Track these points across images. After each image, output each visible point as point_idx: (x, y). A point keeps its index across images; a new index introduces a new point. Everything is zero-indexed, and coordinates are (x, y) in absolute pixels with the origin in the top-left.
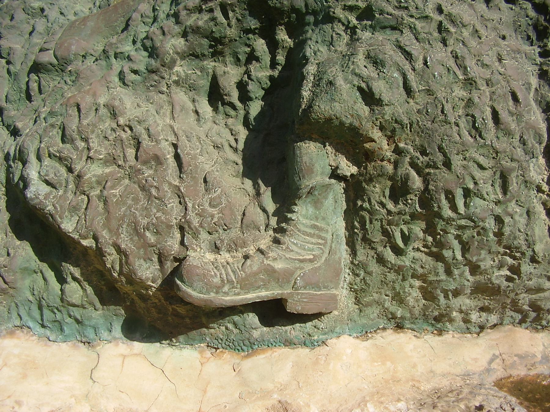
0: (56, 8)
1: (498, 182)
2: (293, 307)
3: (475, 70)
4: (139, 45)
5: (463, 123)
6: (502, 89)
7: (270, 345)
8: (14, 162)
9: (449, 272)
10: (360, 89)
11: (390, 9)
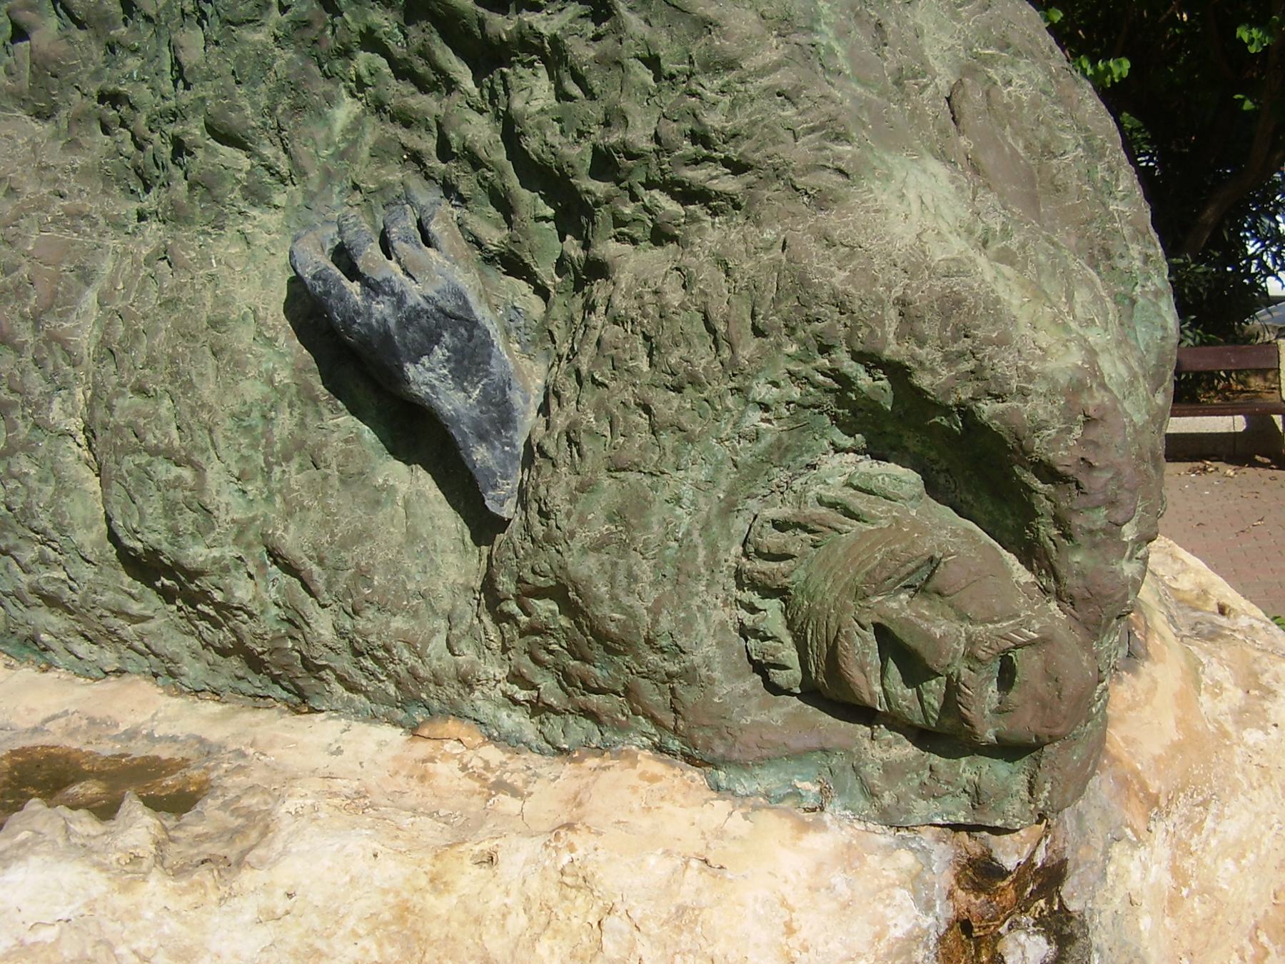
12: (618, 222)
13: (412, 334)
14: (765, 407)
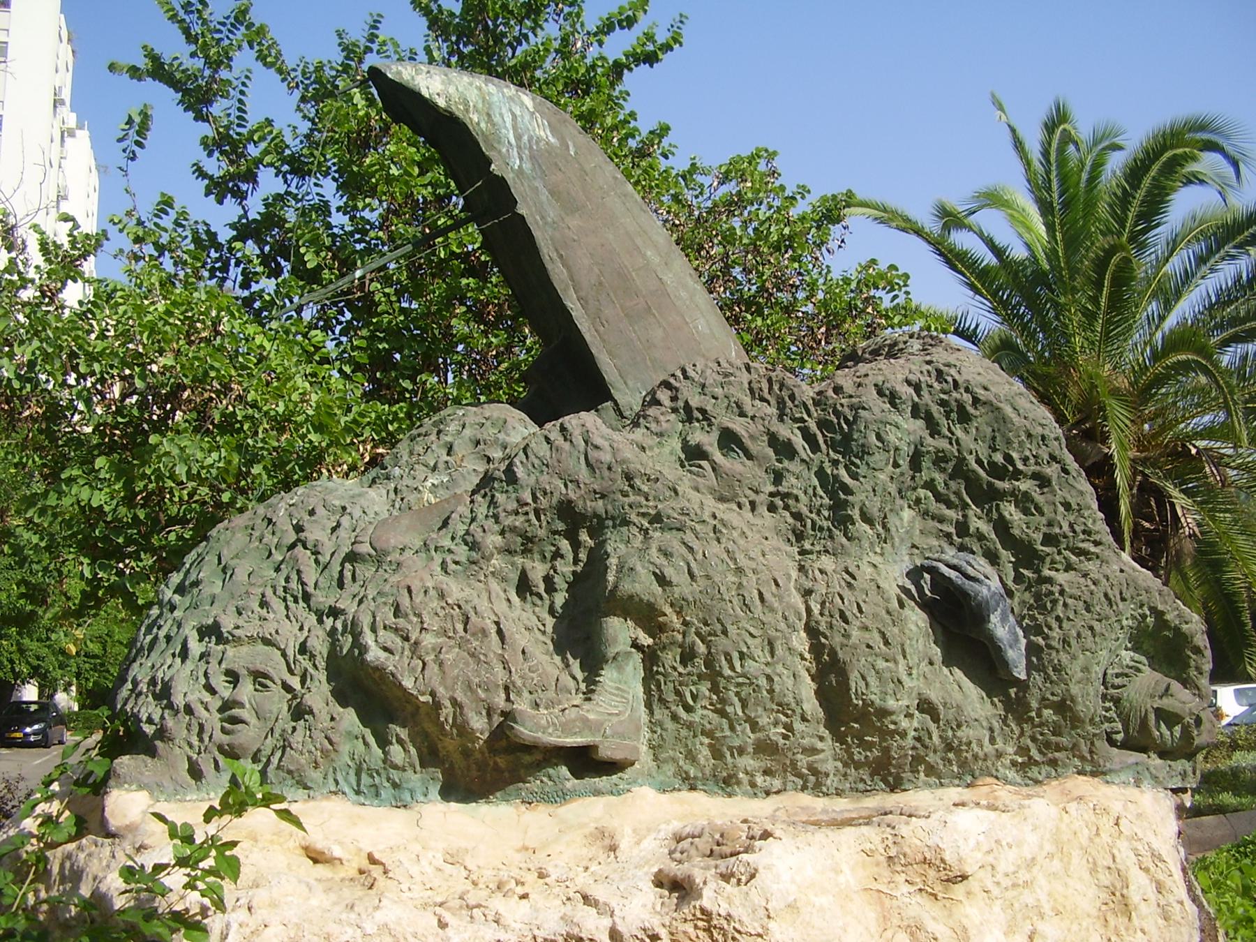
0: (358, 507)
1: (767, 648)
3: (743, 561)
4: (458, 540)
5: (735, 600)
6: (766, 576)
8: (342, 635)
9: (732, 728)
10: (654, 574)
11: (676, 515)
12: (1053, 562)
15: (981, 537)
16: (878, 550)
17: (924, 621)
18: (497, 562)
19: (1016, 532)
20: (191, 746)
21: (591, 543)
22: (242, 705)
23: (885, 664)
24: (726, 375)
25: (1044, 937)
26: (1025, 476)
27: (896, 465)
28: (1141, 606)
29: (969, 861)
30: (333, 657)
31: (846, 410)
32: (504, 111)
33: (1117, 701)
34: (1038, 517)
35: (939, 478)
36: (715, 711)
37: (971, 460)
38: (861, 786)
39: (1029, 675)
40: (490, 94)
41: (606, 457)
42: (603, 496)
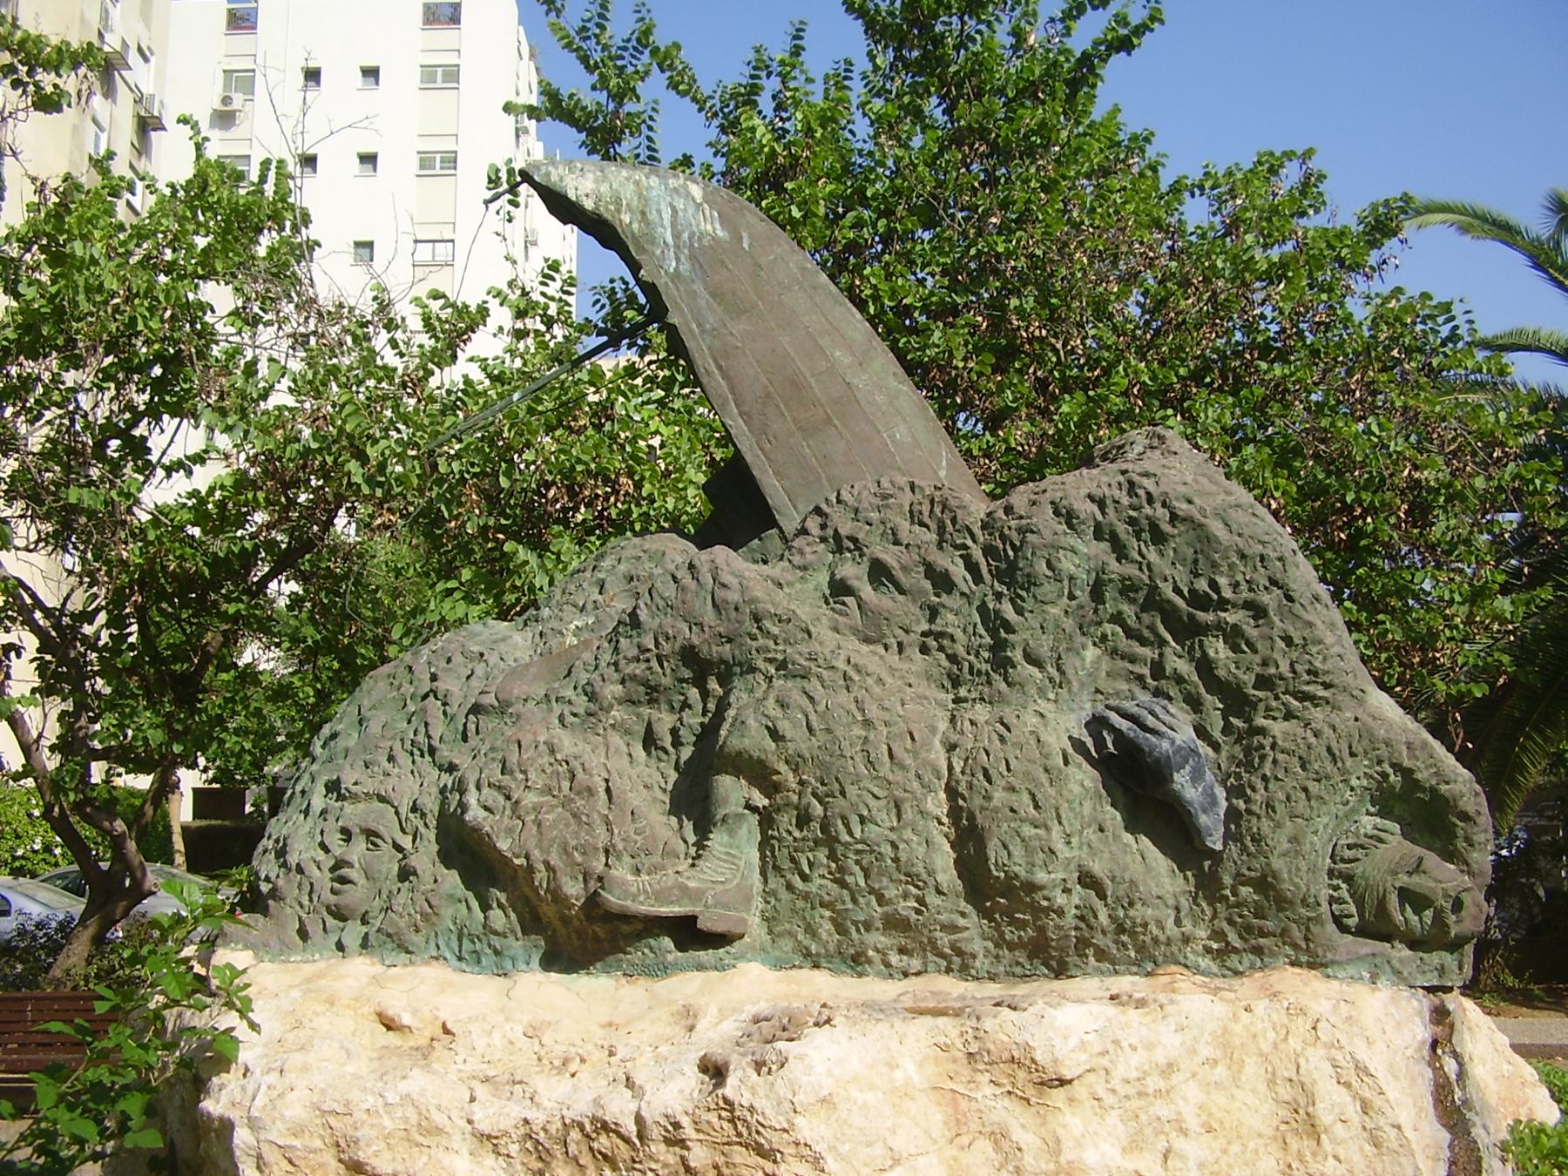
2: (704, 924)
3: (873, 711)
4: (580, 690)
5: (860, 755)
7: (679, 968)
9: (854, 901)
10: (767, 727)
12: (1268, 709)
13: (1178, 759)
14: (1352, 789)
15: (1179, 679)
16: (1052, 696)
17: (1093, 780)
18: (617, 713)
19: (1221, 673)
20: (302, 906)
21: (720, 691)
22: (351, 865)
23: (1034, 831)
24: (885, 497)
25: (1183, 1158)
26: (1234, 606)
27: (1072, 597)
28: (1380, 762)
29: (1067, 1062)
30: (443, 816)
31: (1014, 535)
32: (663, 206)
33: (1349, 879)
34: (1250, 656)
35: (1128, 610)
36: (834, 881)
37: (1167, 590)
38: (1018, 970)
39: (1225, 845)
40: (650, 188)
41: (733, 596)
42: (730, 641)
